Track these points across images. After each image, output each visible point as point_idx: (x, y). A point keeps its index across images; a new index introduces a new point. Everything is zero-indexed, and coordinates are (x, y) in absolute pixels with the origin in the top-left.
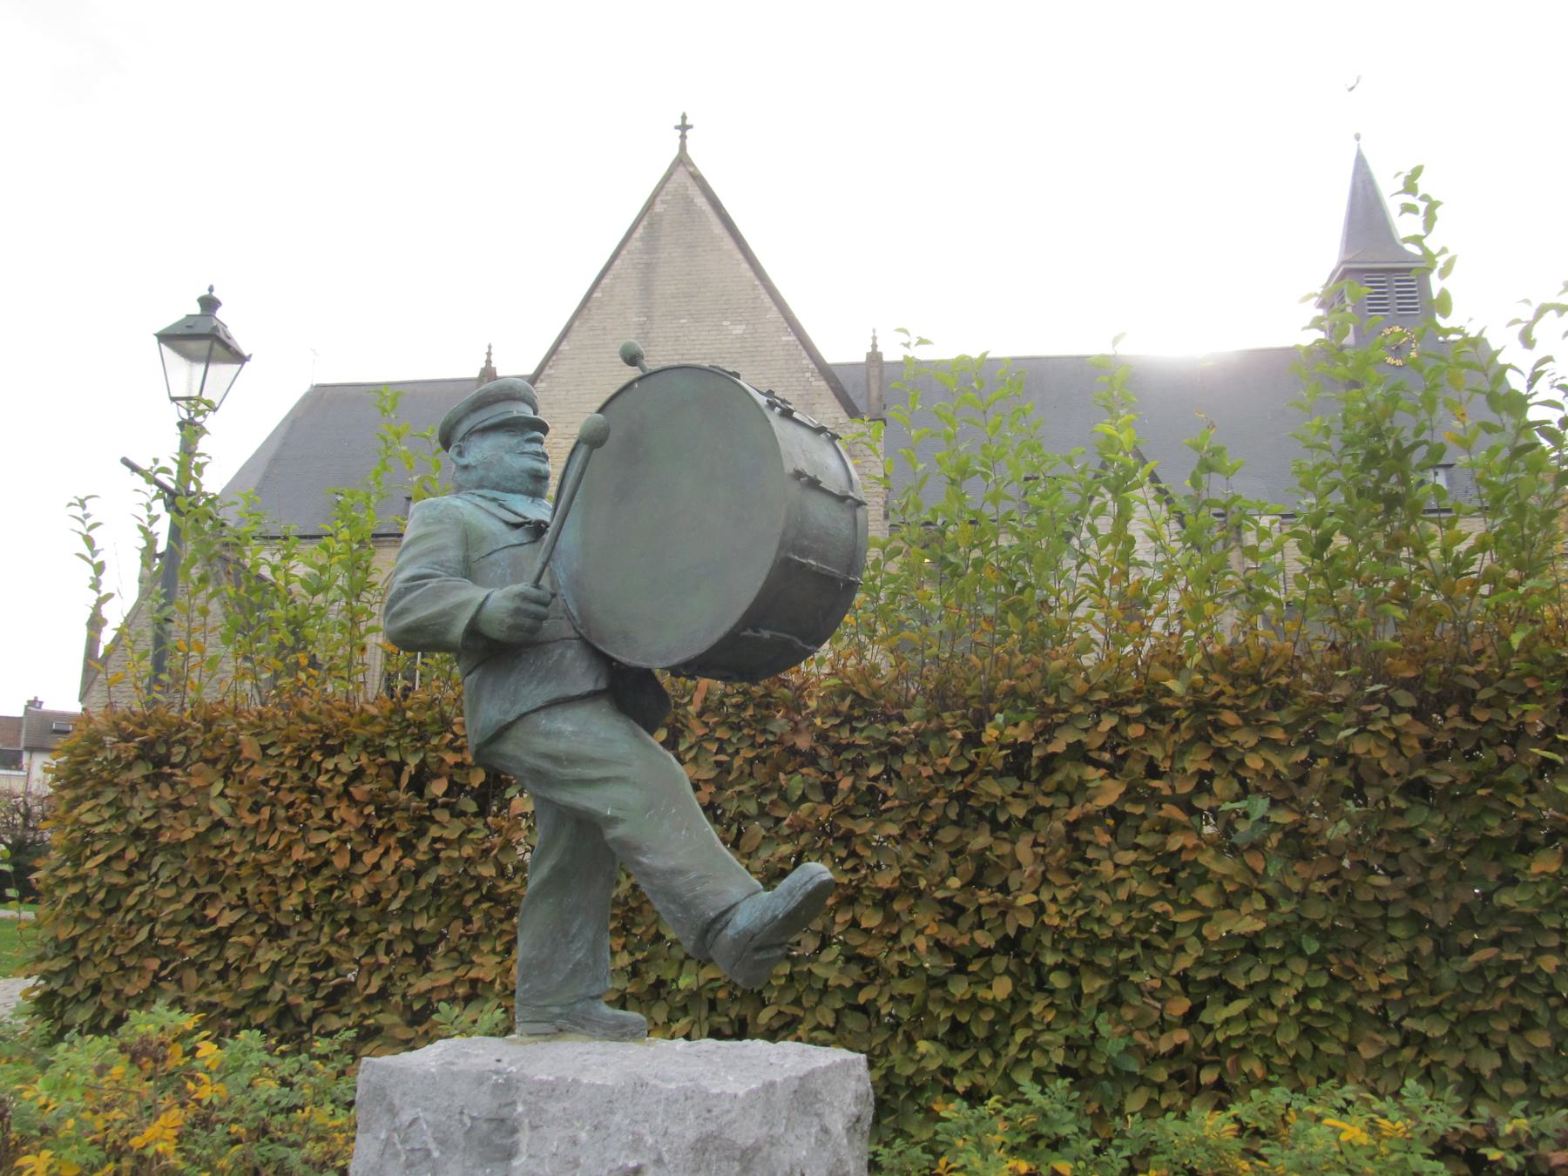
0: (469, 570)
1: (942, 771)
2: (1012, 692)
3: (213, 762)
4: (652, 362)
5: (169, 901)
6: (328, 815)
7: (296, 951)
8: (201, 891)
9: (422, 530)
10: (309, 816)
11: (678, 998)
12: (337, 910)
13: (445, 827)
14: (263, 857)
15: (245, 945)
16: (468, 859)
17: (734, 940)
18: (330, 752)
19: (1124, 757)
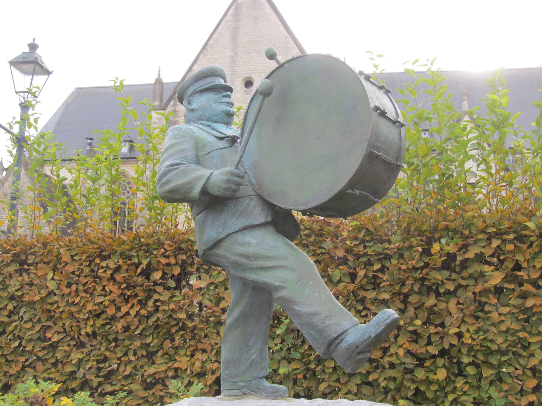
0: (198, 161)
1: (411, 267)
2: (447, 228)
3: (48, 263)
4: (282, 59)
5: (29, 329)
6: (104, 289)
7: (89, 355)
8: (43, 324)
9: (174, 141)
10: (95, 289)
11: (278, 378)
12: (109, 334)
13: (161, 295)
14: (73, 309)
15: (65, 351)
16: (172, 310)
17: (346, 349)
18: (104, 258)
19: (505, 259)
